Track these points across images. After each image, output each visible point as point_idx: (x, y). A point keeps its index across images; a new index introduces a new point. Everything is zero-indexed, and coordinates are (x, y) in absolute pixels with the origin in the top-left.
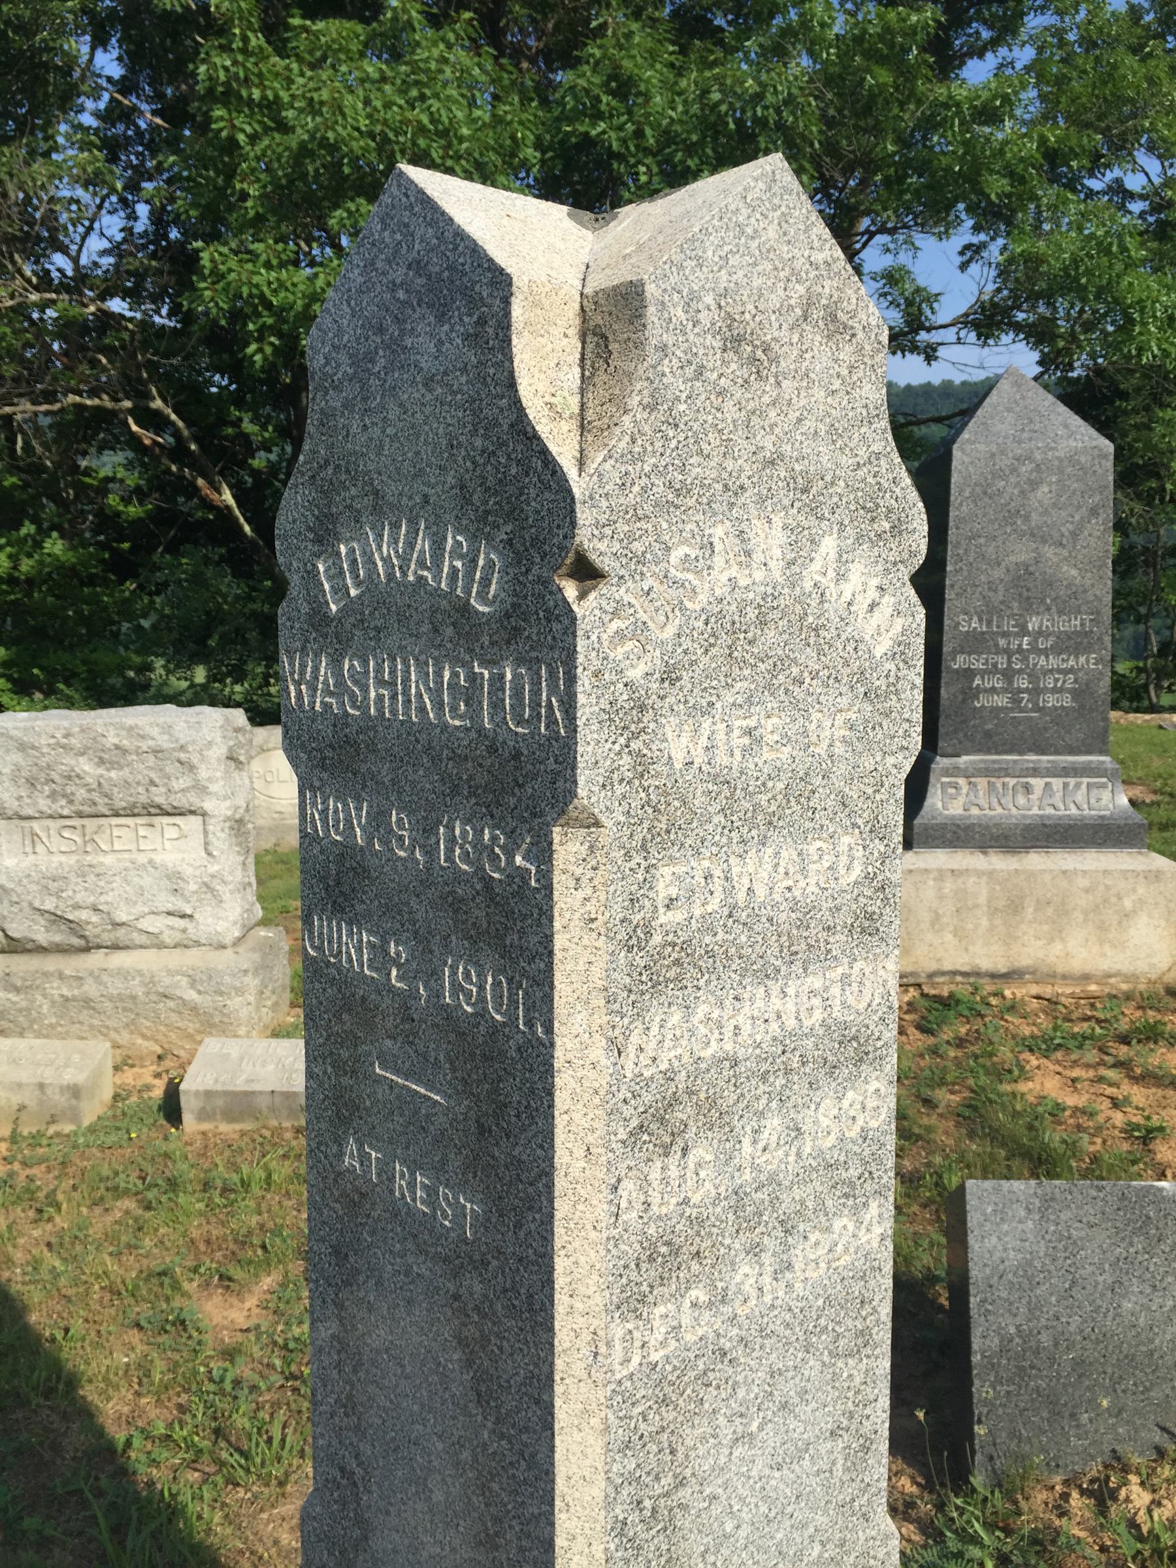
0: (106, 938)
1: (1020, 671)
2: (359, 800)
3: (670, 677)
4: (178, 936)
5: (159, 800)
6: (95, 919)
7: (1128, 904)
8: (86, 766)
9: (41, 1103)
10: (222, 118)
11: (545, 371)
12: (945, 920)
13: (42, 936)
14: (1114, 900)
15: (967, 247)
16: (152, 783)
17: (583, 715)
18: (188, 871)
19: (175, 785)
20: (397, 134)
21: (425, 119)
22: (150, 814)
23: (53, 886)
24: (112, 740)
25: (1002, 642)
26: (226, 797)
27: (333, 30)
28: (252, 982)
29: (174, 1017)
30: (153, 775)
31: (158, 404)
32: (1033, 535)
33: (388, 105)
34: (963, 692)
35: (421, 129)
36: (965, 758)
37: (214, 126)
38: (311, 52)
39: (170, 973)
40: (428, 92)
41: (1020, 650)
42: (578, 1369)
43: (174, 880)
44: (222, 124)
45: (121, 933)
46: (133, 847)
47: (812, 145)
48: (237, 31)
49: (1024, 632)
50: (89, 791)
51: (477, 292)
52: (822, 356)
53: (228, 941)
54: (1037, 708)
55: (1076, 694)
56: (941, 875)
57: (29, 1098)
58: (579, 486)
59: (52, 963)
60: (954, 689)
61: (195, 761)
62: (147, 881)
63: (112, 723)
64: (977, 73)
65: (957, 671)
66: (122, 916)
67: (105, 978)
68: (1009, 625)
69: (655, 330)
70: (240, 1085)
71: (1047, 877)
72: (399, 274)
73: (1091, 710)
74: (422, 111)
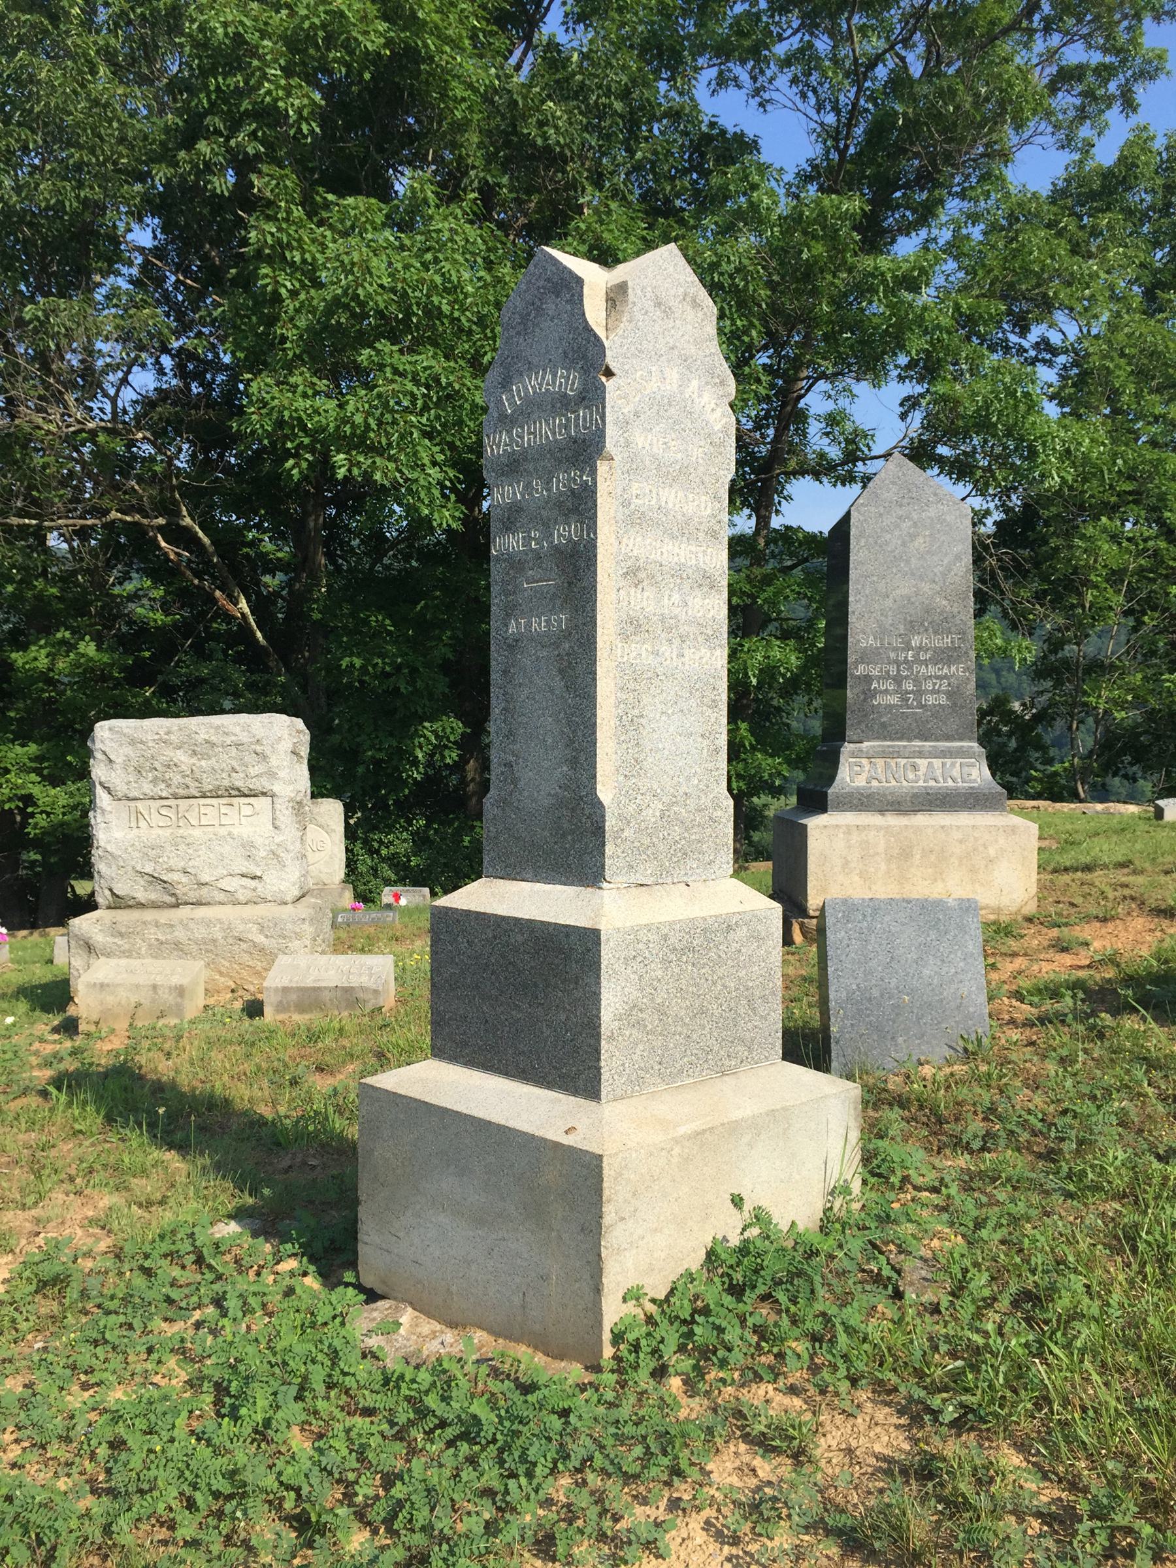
0: (193, 896)
1: (907, 677)
2: (518, 483)
3: (637, 415)
4: (249, 895)
5: (238, 784)
6: (184, 879)
7: (992, 852)
8: (181, 757)
9: (153, 1001)
10: (267, 276)
11: (594, 311)
12: (853, 865)
13: (141, 896)
14: (981, 849)
15: (908, 398)
16: (234, 770)
17: (608, 419)
18: (259, 841)
19: (253, 771)
20: (414, 291)
21: (438, 279)
22: (230, 796)
23: (152, 853)
24: (203, 736)
25: (892, 655)
26: (291, 782)
27: (361, 204)
28: (308, 929)
29: (246, 957)
30: (234, 763)
31: (187, 521)
32: (913, 574)
33: (407, 267)
34: (864, 692)
35: (433, 287)
36: (866, 744)
37: (260, 283)
38: (342, 221)
39: (244, 921)
40: (441, 256)
41: (906, 661)
42: (605, 655)
43: (248, 849)
44: (268, 280)
45: (204, 891)
46: (216, 822)
47: (760, 306)
48: (283, 204)
49: (908, 647)
50: (184, 777)
51: (572, 285)
52: (690, 314)
53: (289, 898)
54: (922, 707)
55: (950, 695)
56: (848, 830)
57: (144, 997)
58: (606, 343)
59: (149, 915)
60: (856, 691)
61: (268, 753)
62: (226, 849)
63: (201, 726)
64: (906, 247)
65: (859, 677)
66: (205, 878)
67: (192, 925)
68: (897, 643)
69: (631, 296)
70: (309, 983)
71: (930, 831)
72: (541, 283)
73: (962, 707)
74: (436, 272)
